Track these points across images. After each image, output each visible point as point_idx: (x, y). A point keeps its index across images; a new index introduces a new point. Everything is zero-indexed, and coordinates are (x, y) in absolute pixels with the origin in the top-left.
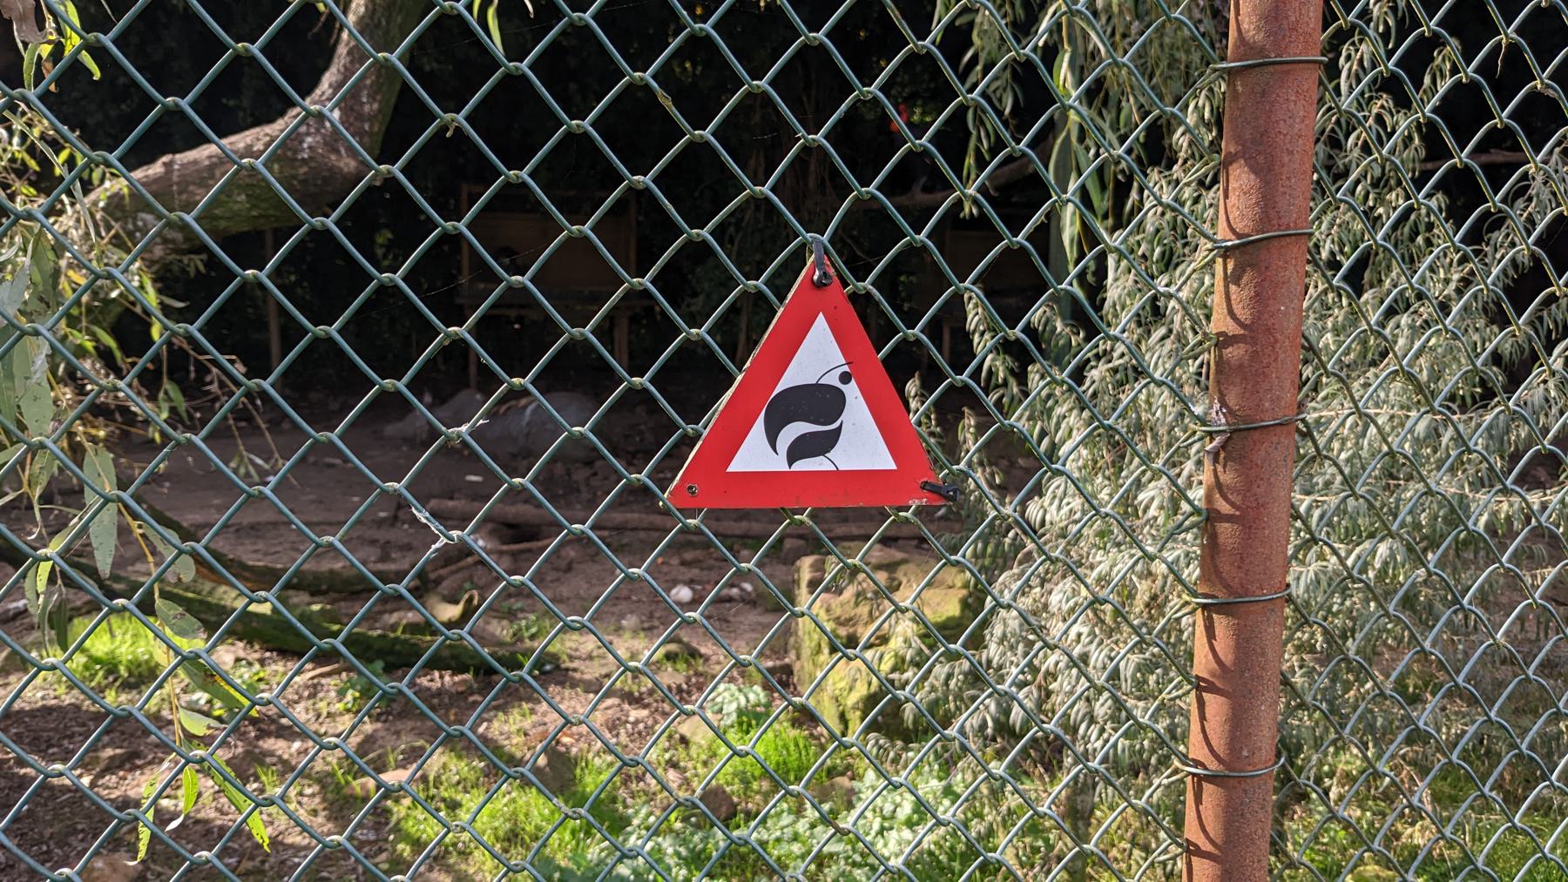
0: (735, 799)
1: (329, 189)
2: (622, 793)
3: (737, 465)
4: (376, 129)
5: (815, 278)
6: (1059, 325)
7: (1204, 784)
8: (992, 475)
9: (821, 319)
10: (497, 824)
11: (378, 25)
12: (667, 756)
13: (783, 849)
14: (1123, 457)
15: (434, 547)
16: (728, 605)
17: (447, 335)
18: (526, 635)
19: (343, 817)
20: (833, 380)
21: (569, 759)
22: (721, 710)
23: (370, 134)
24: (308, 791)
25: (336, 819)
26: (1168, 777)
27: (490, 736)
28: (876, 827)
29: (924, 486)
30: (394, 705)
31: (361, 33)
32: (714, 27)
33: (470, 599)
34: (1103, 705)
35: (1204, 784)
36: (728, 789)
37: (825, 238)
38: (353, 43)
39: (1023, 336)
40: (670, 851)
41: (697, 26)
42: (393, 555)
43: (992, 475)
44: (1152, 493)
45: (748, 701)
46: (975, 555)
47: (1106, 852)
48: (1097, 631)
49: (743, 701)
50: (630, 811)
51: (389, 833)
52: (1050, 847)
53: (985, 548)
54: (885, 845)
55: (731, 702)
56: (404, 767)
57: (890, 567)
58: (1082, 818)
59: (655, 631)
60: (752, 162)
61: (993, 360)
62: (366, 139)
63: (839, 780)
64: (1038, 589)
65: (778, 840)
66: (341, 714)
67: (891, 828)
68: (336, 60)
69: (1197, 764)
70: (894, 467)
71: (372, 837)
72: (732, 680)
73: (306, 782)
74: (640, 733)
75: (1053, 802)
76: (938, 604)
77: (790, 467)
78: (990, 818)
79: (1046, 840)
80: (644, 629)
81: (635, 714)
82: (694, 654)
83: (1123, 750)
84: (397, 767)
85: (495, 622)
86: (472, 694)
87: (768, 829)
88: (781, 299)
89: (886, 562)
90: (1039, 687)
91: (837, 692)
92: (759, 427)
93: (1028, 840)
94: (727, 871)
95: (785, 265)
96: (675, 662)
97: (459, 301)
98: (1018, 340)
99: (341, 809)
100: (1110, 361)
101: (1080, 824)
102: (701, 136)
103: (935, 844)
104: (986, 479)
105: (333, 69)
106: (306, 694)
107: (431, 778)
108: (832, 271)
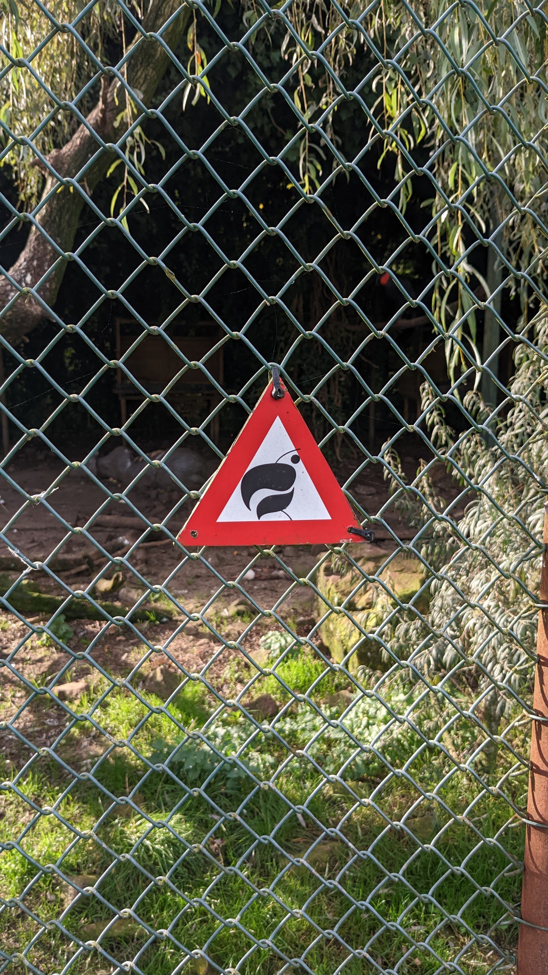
0: (278, 703)
1: (25, 325)
2: (208, 698)
3: (223, 518)
4: (54, 287)
5: (273, 393)
6: (482, 406)
7: (542, 726)
8: (438, 501)
9: (278, 420)
10: (131, 717)
11: (54, 221)
12: (236, 675)
13: (306, 735)
14: (522, 492)
15: (25, 572)
16: (277, 581)
17: (29, 435)
18: (152, 599)
19: (39, 711)
20: (287, 461)
21: (176, 677)
22: (269, 648)
23: (50, 290)
24: (19, 695)
25: (35, 712)
26: (518, 721)
27: (129, 661)
28: (364, 722)
29: (350, 530)
30: (72, 642)
31: (43, 227)
32: (204, 226)
33: (117, 578)
34: (503, 651)
35: (542, 726)
36: (273, 697)
37: (281, 366)
38: (38, 233)
39: (419, 429)
40: (236, 735)
41: (192, 225)
42: (74, 549)
43: (438, 501)
44: (538, 516)
45: (286, 642)
46: (427, 555)
47: (510, 741)
48: (500, 604)
49: (283, 642)
50: (212, 710)
51: (66, 721)
52: (475, 738)
53: (433, 550)
54: (370, 734)
55: (276, 642)
56: (76, 681)
57: (377, 559)
58: (494, 720)
59: (231, 597)
60: (295, 301)
61: (438, 429)
62: (48, 294)
63: (343, 692)
64: (464, 577)
65: (303, 730)
66: (40, 647)
67: (374, 724)
68: (28, 244)
69: (538, 713)
70: (330, 518)
71: (56, 723)
72: (277, 629)
73: (17, 689)
74: (220, 661)
75: (475, 709)
76: (406, 583)
77: (259, 518)
78: (436, 719)
79: (472, 733)
80: (224, 596)
81: (218, 649)
82: (255, 612)
83: (515, 681)
84: (72, 681)
85: (133, 591)
86: (118, 636)
87: (297, 722)
88: (252, 406)
89: (373, 556)
90: (464, 640)
91: (342, 637)
92: (237, 492)
93: (461, 732)
94: (272, 748)
95: (254, 384)
96: (243, 617)
97: (115, 391)
98: (415, 432)
99: (38, 706)
100: (513, 430)
101: (493, 724)
102: (196, 299)
103: (402, 734)
104: (435, 505)
105: (27, 250)
106: (19, 634)
107: (92, 688)
108: (285, 388)
